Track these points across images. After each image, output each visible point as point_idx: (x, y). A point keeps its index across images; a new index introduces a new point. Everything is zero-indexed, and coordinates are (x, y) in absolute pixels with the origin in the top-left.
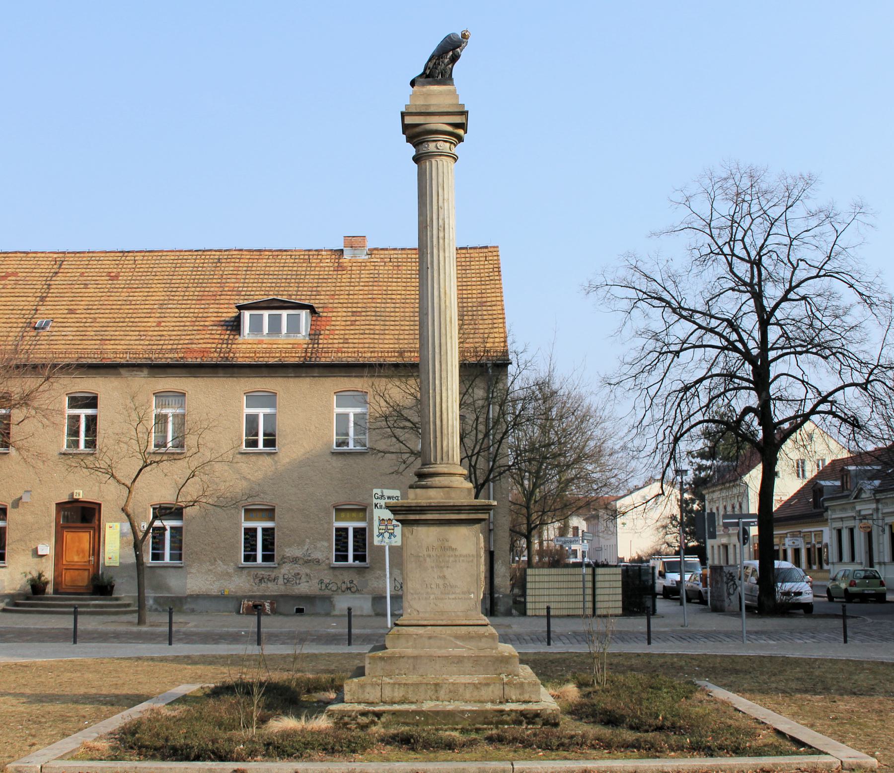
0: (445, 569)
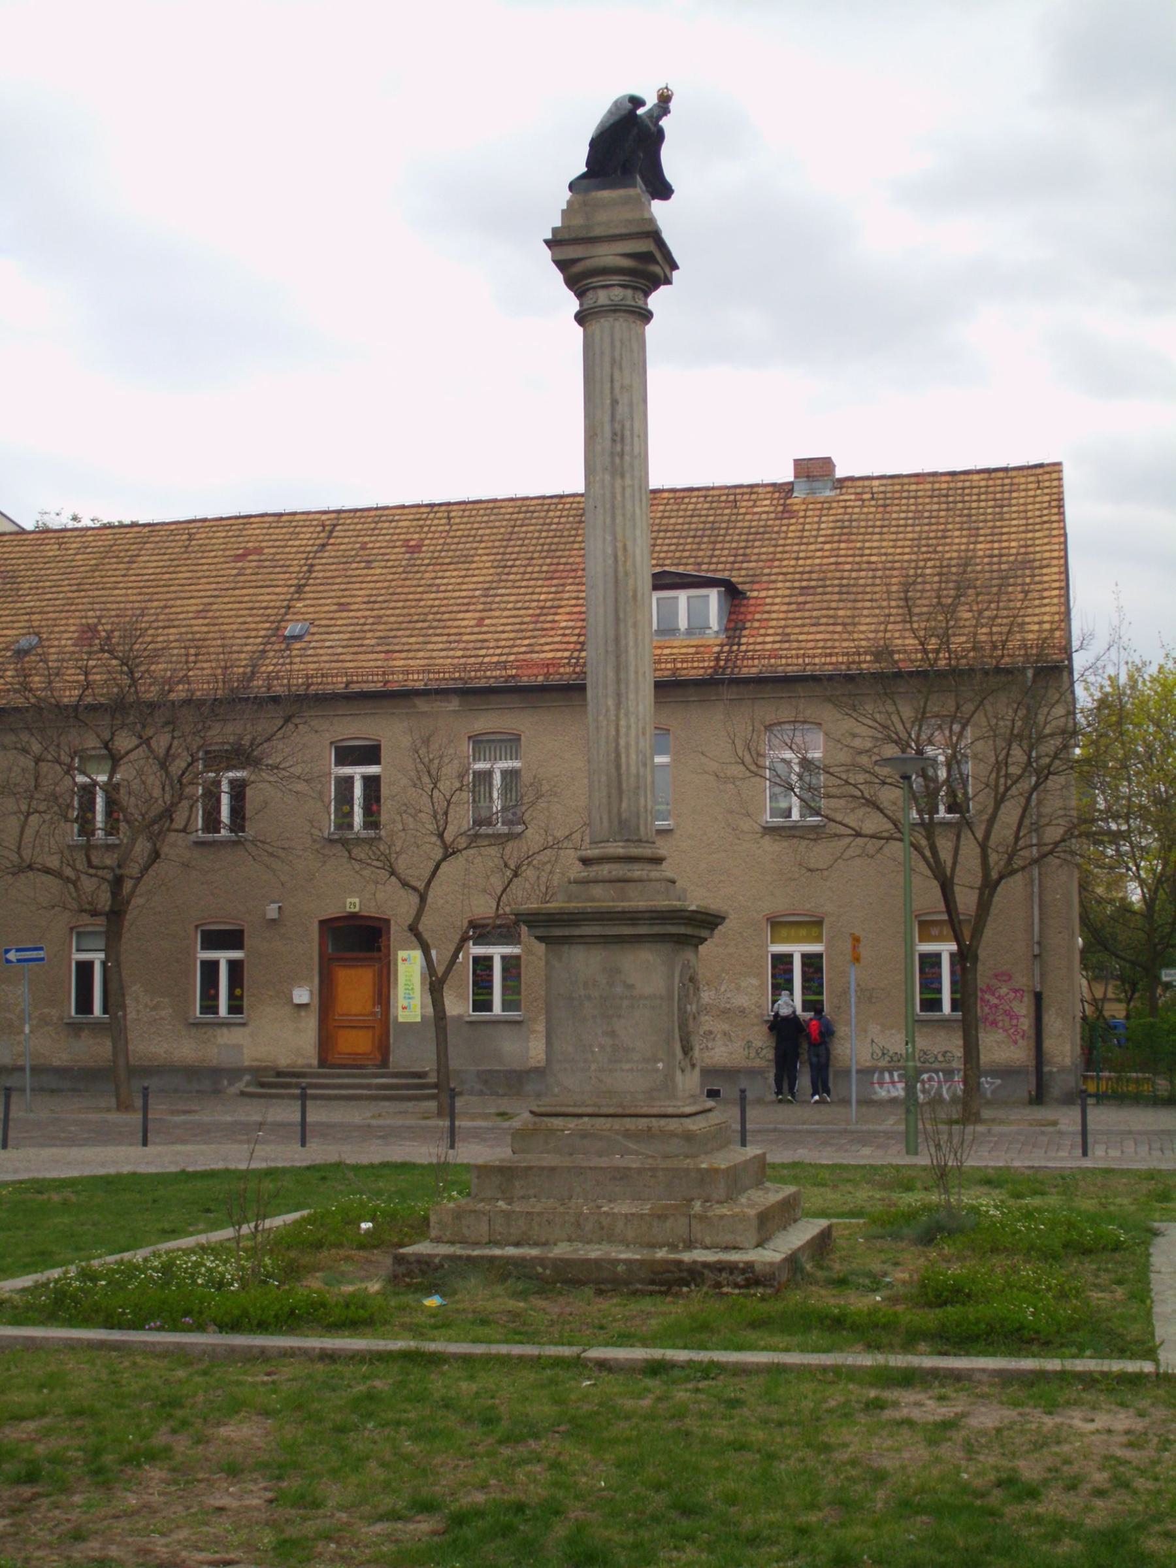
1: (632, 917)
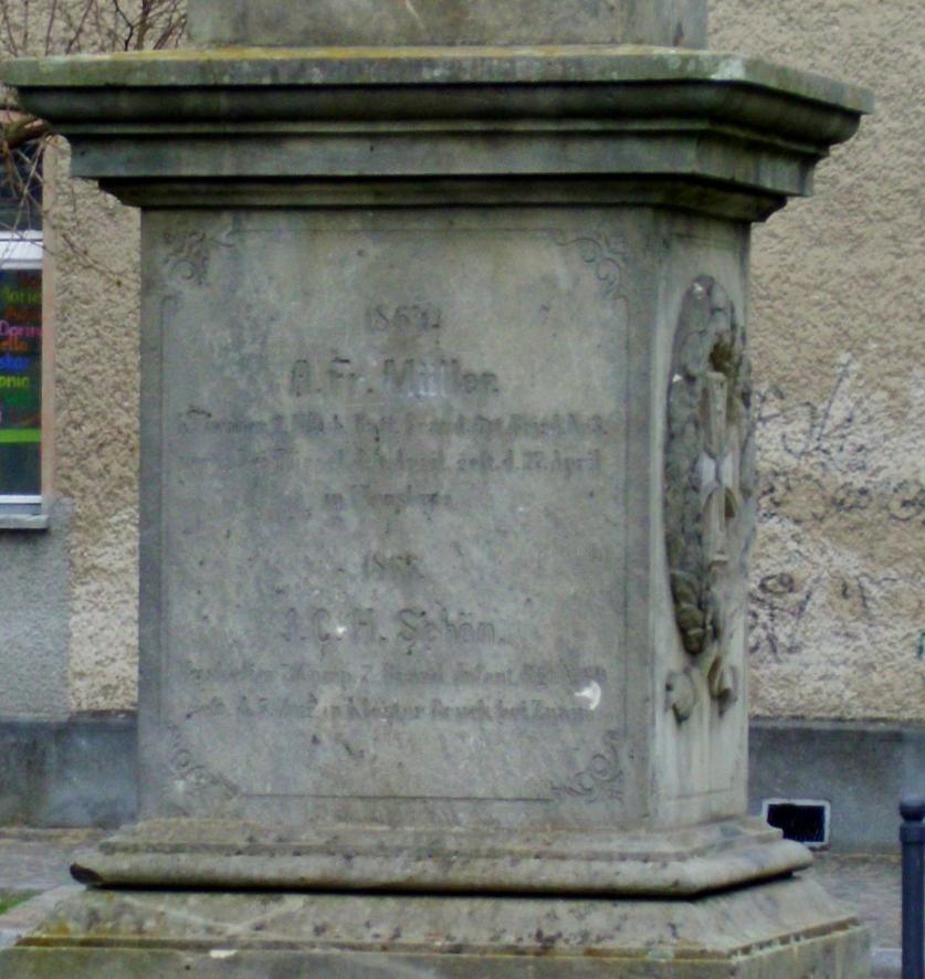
0: (413, 513)
1: (487, 107)
